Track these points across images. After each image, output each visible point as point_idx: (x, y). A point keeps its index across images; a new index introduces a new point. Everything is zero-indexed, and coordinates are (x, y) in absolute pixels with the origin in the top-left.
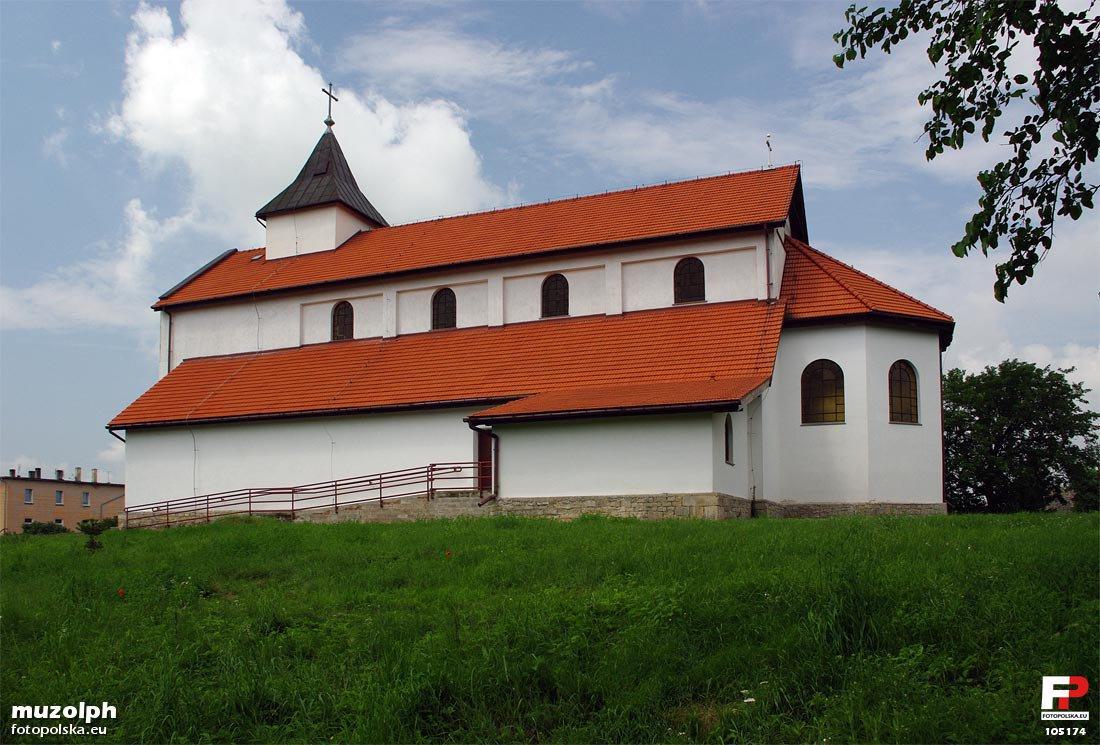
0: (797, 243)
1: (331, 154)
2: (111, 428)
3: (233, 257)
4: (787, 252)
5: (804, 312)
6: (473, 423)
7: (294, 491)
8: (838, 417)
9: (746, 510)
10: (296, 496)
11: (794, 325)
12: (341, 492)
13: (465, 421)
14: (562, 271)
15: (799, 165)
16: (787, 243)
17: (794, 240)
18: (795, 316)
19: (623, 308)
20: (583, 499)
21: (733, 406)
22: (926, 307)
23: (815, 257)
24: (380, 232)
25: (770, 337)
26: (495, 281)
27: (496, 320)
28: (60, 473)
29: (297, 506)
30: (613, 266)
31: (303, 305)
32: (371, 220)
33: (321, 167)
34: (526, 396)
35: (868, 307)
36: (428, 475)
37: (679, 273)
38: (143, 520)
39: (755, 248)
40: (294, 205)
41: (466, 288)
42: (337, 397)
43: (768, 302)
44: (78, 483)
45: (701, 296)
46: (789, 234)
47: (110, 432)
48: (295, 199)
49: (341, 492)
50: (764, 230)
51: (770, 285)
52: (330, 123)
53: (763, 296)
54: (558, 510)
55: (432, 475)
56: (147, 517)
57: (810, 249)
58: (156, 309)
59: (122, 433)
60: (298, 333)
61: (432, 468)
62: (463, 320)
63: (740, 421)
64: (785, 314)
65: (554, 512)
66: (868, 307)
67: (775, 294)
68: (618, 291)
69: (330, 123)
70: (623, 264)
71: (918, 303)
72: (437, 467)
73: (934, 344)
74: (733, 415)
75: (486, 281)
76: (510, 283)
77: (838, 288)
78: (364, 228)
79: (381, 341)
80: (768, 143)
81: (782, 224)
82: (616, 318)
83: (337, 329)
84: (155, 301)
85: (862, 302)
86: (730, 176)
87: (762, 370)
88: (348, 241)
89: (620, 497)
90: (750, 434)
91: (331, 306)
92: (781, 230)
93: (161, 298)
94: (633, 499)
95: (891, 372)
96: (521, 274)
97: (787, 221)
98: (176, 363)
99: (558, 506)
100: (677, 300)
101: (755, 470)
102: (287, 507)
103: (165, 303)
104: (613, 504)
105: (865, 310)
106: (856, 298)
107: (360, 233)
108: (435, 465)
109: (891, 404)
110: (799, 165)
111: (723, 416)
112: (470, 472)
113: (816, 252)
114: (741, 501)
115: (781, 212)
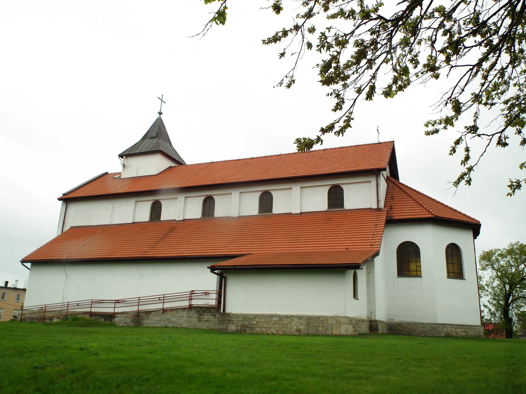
0: (393, 179)
1: (160, 128)
2: (23, 261)
3: (105, 176)
4: (388, 184)
5: (397, 216)
6: (213, 269)
7: (118, 302)
8: (417, 274)
9: (364, 329)
10: (117, 305)
11: (391, 222)
12: (168, 301)
13: (208, 268)
14: (160, 199)
15: (394, 141)
16: (387, 180)
17: (391, 179)
18: (395, 218)
19: (300, 211)
20: (272, 316)
21: (356, 267)
22: (464, 215)
23: (402, 187)
24: (181, 167)
25: (378, 228)
26: (235, 194)
27: (296, 210)
28: (7, 283)
29: (117, 310)
30: (296, 189)
31: (186, 197)
32: (179, 162)
33: (154, 134)
34: (246, 254)
35: (432, 214)
36: (190, 297)
37: (330, 193)
38: (32, 315)
39: (370, 182)
40: (138, 152)
41: (221, 197)
42: (146, 251)
43: (378, 209)
44: (15, 289)
45: (342, 205)
46: (389, 175)
47: (22, 264)
48: (140, 148)
49: (168, 301)
50: (375, 172)
51: (378, 201)
52: (160, 113)
53: (375, 206)
54: (257, 322)
55: (192, 296)
56: (34, 313)
57: (400, 183)
58: (60, 199)
59: (29, 265)
60: (132, 216)
61: (192, 292)
62: (164, 217)
63: (362, 274)
64: (387, 216)
65: (255, 323)
66: (432, 214)
67: (382, 205)
68: (299, 201)
69: (160, 113)
70: (301, 188)
71: (460, 213)
72: (195, 292)
73: (470, 234)
74: (358, 271)
75: (291, 188)
76: (243, 195)
77: (415, 204)
78: (173, 165)
79: (175, 222)
80: (377, 130)
81: (385, 169)
82: (297, 215)
83: (153, 214)
84: (60, 195)
85: (429, 212)
86: (357, 146)
87: (374, 246)
88: (164, 171)
89: (292, 316)
90: (368, 282)
91: (259, 194)
92: (384, 172)
93: (64, 195)
94: (300, 317)
95: (446, 249)
96: (166, 198)
97: (388, 168)
98: (66, 228)
99: (257, 319)
100: (260, 212)
101: (371, 302)
102: (111, 310)
103: (65, 197)
104: (288, 320)
105: (430, 216)
106: (426, 209)
107: (171, 167)
108: (194, 291)
109: (448, 267)
110: (394, 141)
111: (351, 273)
112: (214, 296)
113: (403, 185)
114: (362, 321)
115: (385, 163)
